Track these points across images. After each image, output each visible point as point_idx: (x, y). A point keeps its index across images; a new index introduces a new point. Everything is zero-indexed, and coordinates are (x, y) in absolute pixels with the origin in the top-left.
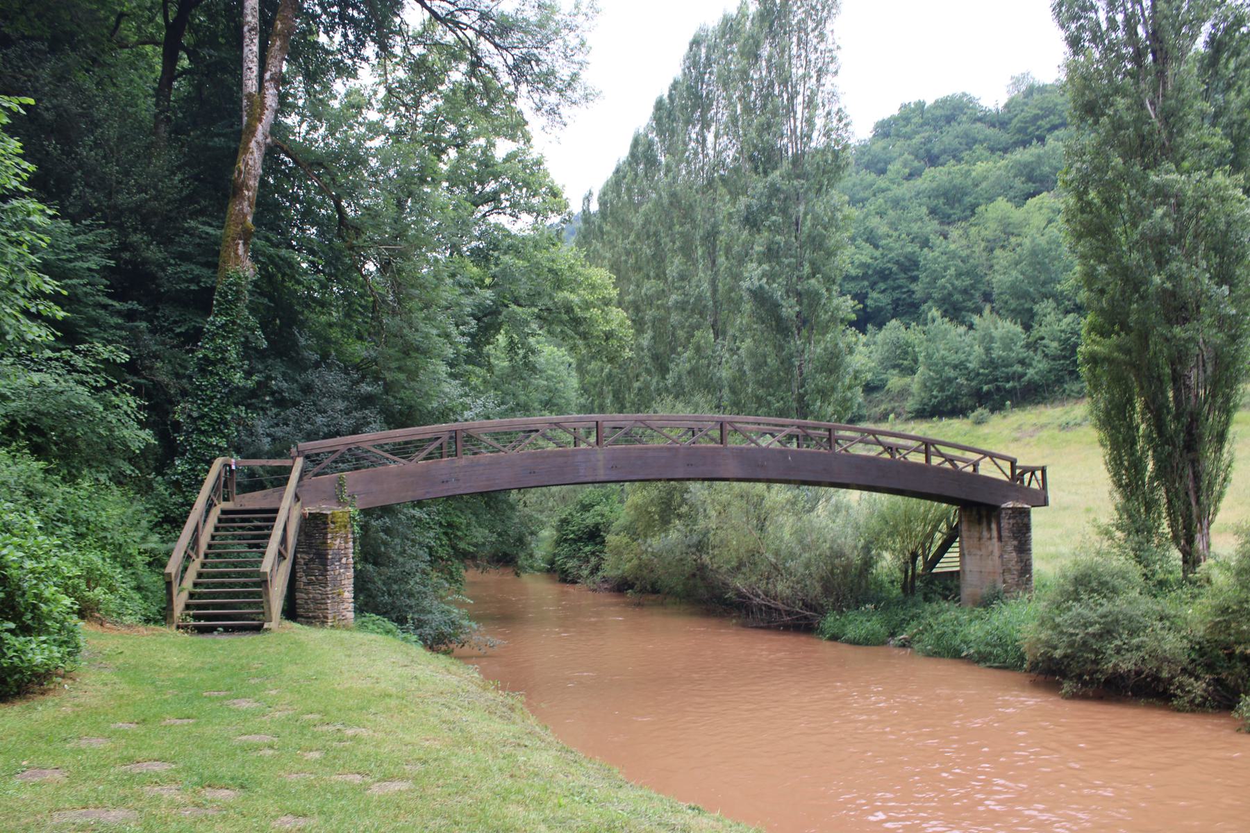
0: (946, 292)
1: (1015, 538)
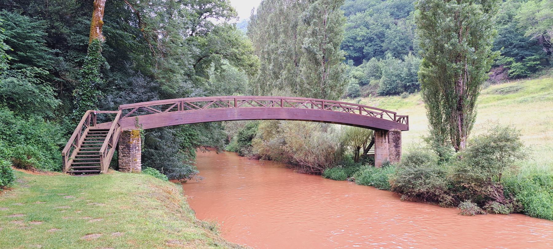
0: (395, 46)
1: (394, 142)
